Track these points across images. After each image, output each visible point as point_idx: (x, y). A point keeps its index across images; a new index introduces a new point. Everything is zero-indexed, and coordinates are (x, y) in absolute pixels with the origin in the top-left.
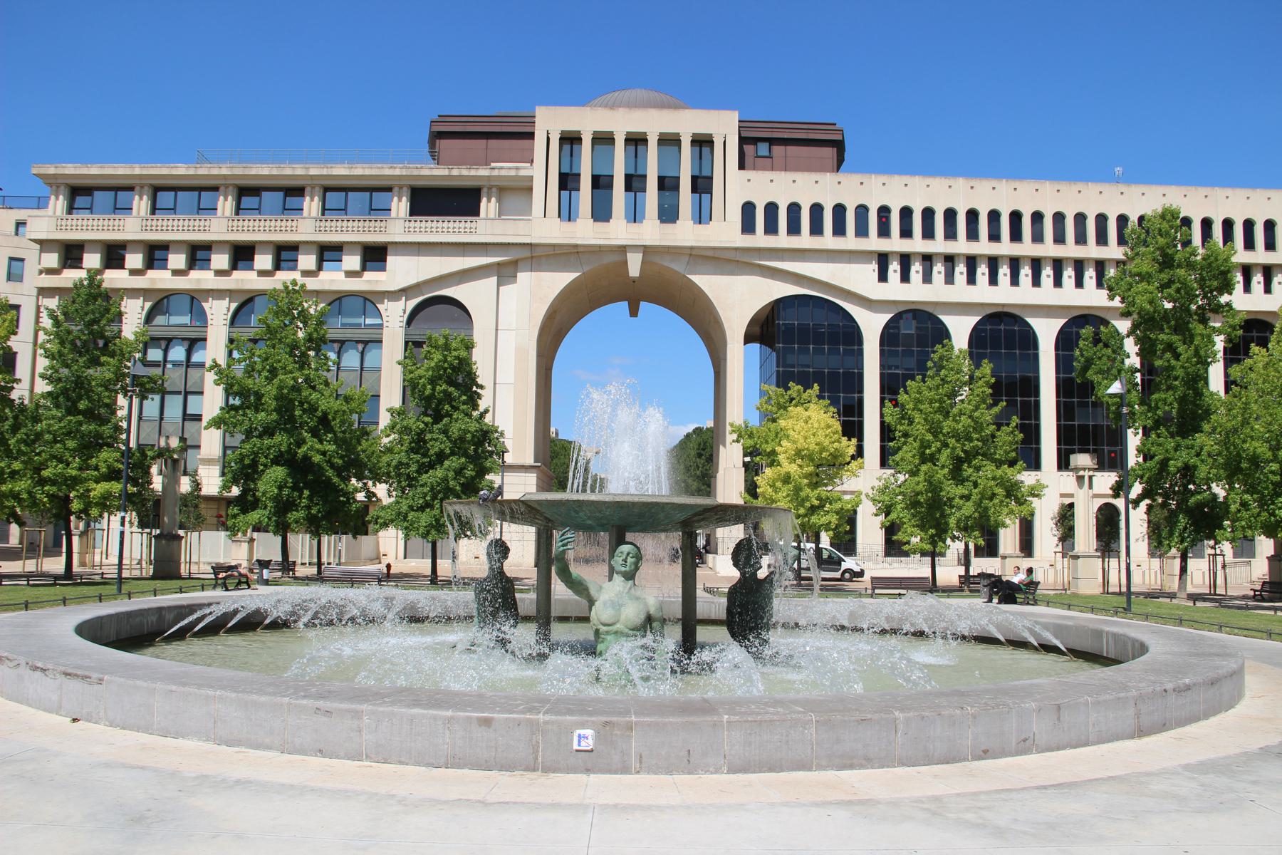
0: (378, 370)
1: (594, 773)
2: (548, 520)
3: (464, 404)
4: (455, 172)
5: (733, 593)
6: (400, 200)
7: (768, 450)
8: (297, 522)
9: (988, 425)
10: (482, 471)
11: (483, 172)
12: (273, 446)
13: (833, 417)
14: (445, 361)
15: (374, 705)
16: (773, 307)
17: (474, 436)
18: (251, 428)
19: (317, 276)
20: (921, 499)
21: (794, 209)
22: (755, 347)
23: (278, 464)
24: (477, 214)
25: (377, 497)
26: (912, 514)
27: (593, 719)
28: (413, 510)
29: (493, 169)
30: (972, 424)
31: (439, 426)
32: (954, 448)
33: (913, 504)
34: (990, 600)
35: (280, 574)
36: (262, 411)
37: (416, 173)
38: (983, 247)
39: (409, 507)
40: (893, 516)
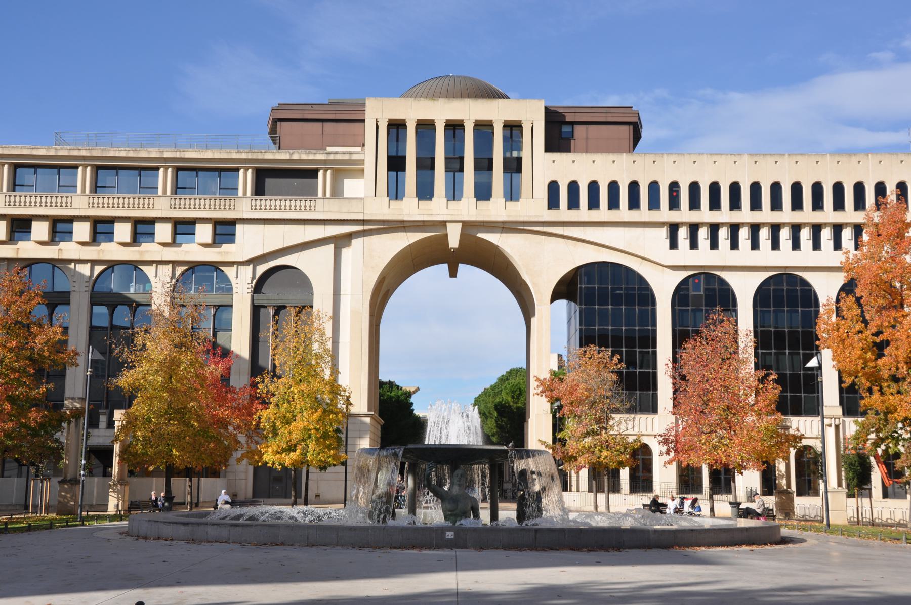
4: (296, 157)
22: (562, 303)
29: (329, 153)
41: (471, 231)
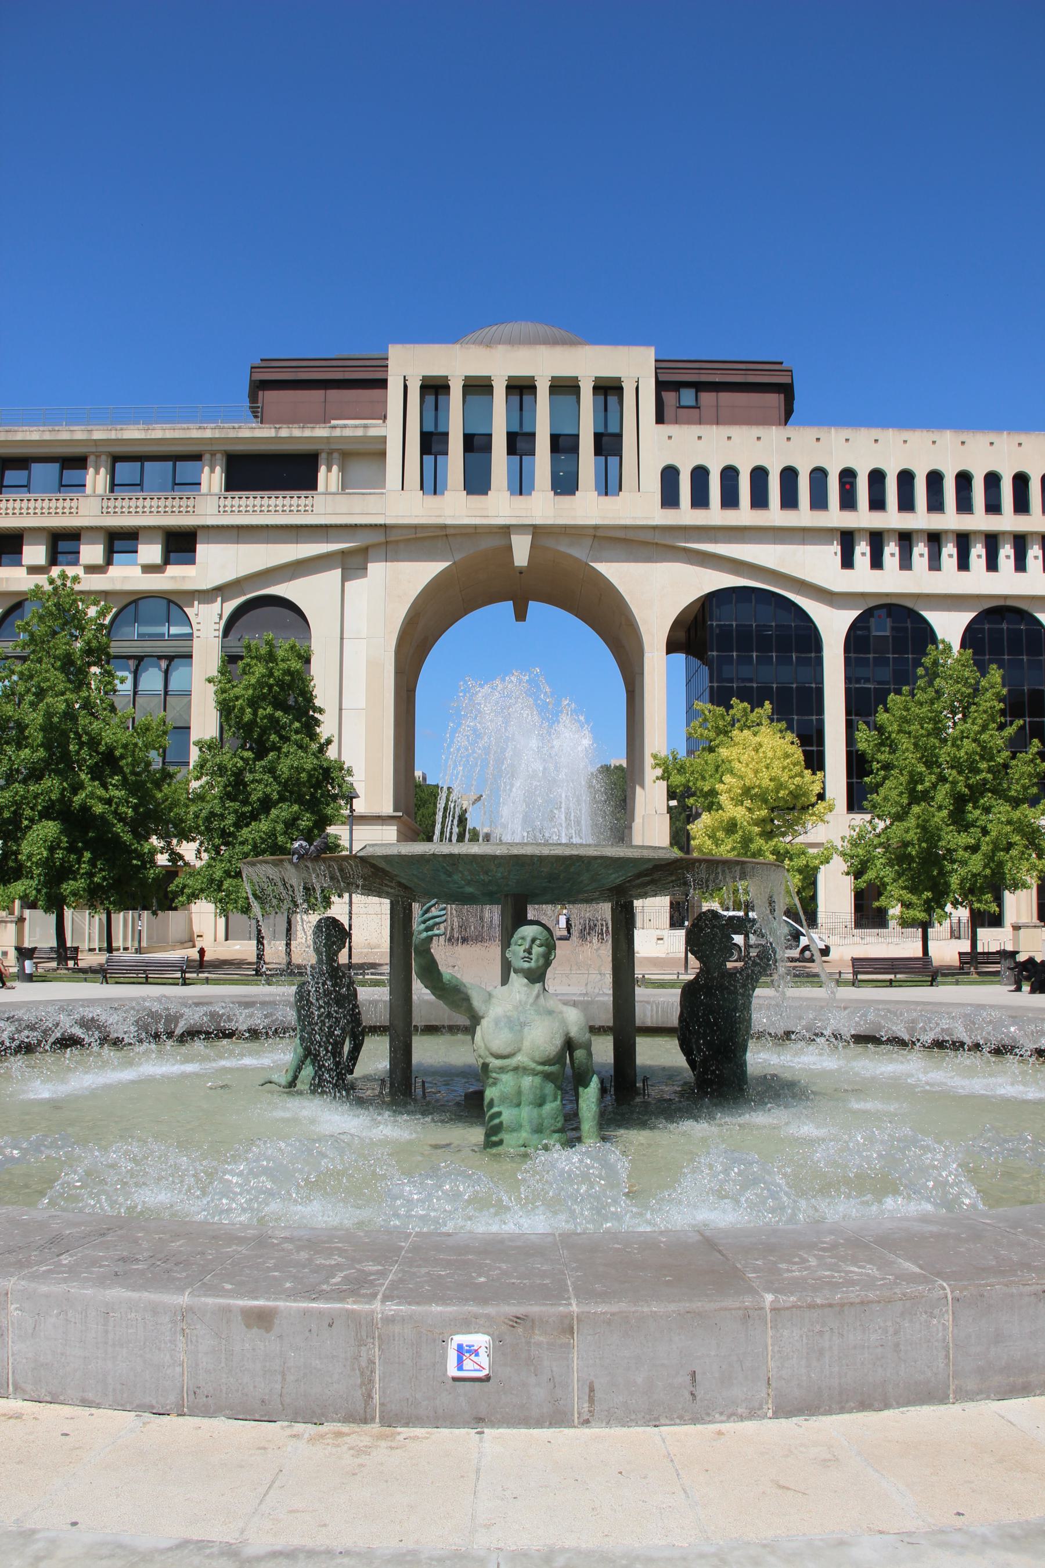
0: (188, 694)
1: (493, 1425)
2: (406, 888)
3: (297, 732)
4: (284, 433)
5: (690, 991)
6: (212, 471)
7: (706, 789)
8: (74, 894)
9: (999, 752)
10: (323, 821)
11: (321, 432)
12: (42, 794)
13: (792, 743)
14: (271, 674)
15: (34, 1277)
16: (703, 605)
17: (310, 776)
18: (11, 769)
19: (105, 572)
20: (913, 851)
21: (730, 474)
22: (680, 658)
23: (49, 818)
24: (313, 486)
25: (184, 860)
26: (897, 872)
27: (490, 1310)
28: (230, 876)
29: (334, 427)
30: (978, 749)
31: (263, 763)
32: (954, 783)
33: (900, 858)
34: (1019, 989)
35: (54, 964)
36: (26, 747)
37: (232, 434)
38: (979, 521)
39: (225, 872)
40: (870, 875)
41: (550, 543)
